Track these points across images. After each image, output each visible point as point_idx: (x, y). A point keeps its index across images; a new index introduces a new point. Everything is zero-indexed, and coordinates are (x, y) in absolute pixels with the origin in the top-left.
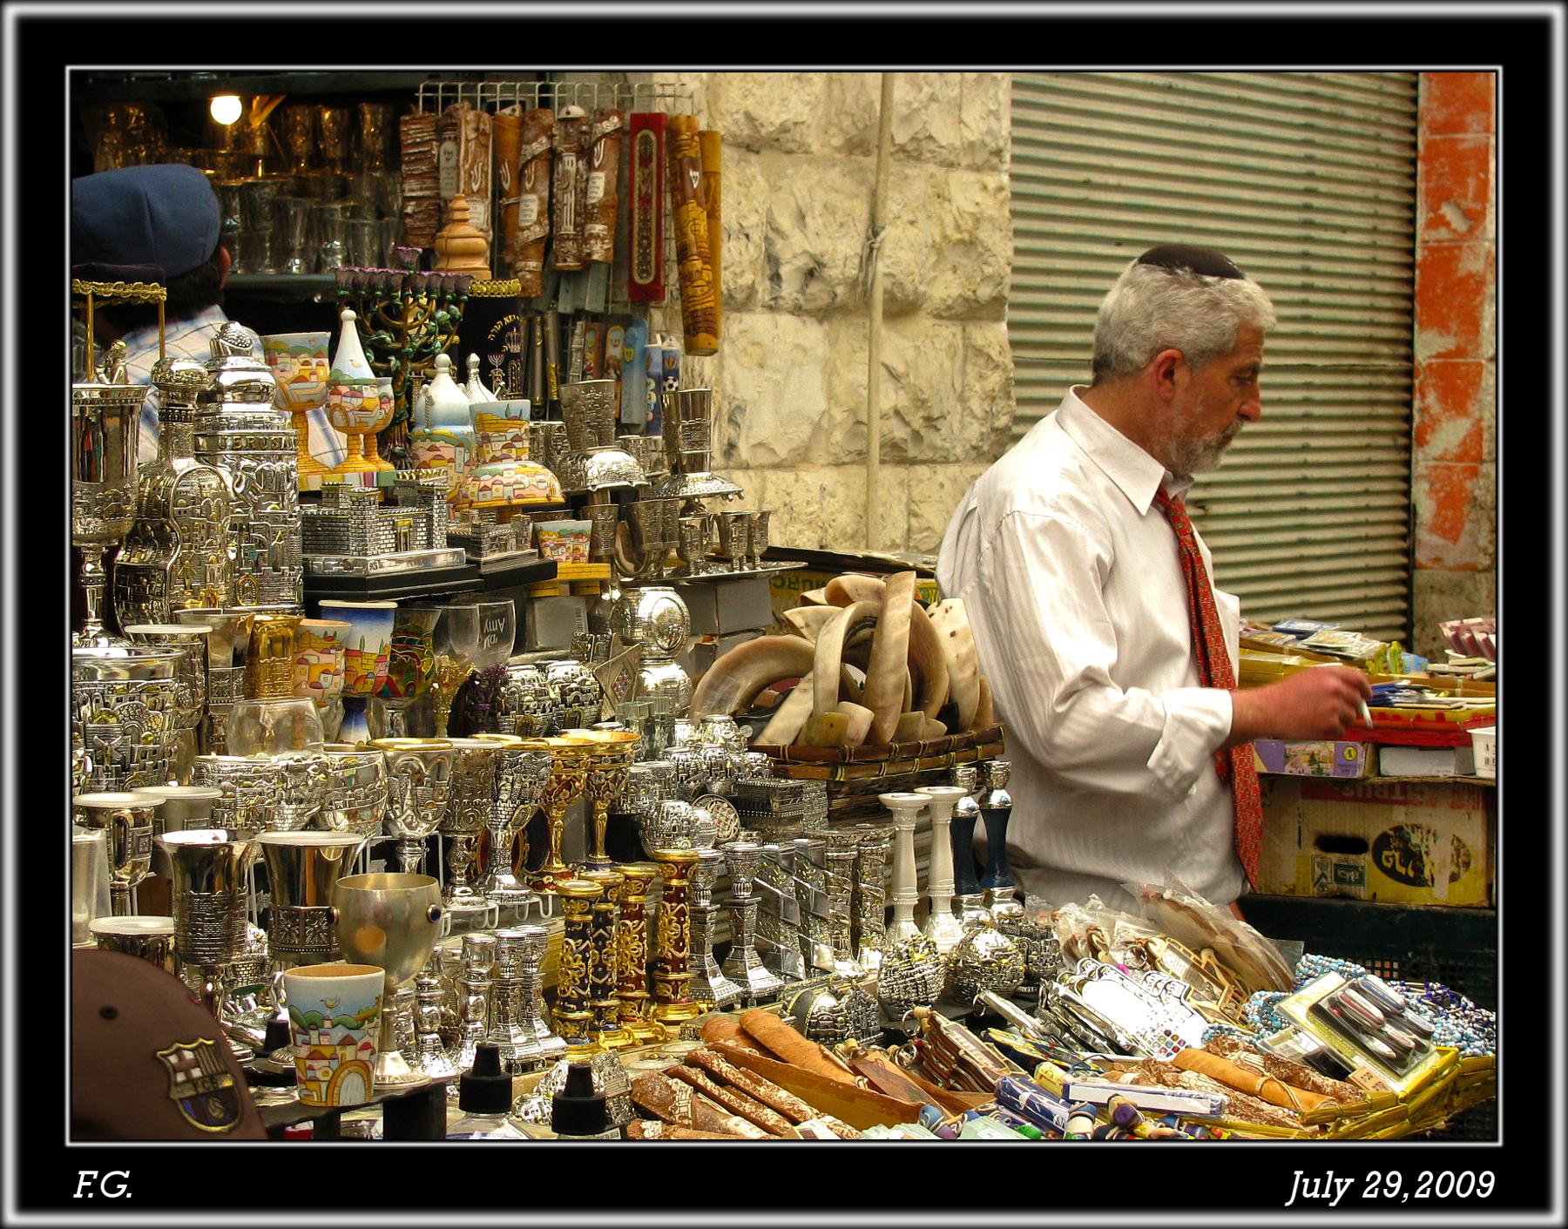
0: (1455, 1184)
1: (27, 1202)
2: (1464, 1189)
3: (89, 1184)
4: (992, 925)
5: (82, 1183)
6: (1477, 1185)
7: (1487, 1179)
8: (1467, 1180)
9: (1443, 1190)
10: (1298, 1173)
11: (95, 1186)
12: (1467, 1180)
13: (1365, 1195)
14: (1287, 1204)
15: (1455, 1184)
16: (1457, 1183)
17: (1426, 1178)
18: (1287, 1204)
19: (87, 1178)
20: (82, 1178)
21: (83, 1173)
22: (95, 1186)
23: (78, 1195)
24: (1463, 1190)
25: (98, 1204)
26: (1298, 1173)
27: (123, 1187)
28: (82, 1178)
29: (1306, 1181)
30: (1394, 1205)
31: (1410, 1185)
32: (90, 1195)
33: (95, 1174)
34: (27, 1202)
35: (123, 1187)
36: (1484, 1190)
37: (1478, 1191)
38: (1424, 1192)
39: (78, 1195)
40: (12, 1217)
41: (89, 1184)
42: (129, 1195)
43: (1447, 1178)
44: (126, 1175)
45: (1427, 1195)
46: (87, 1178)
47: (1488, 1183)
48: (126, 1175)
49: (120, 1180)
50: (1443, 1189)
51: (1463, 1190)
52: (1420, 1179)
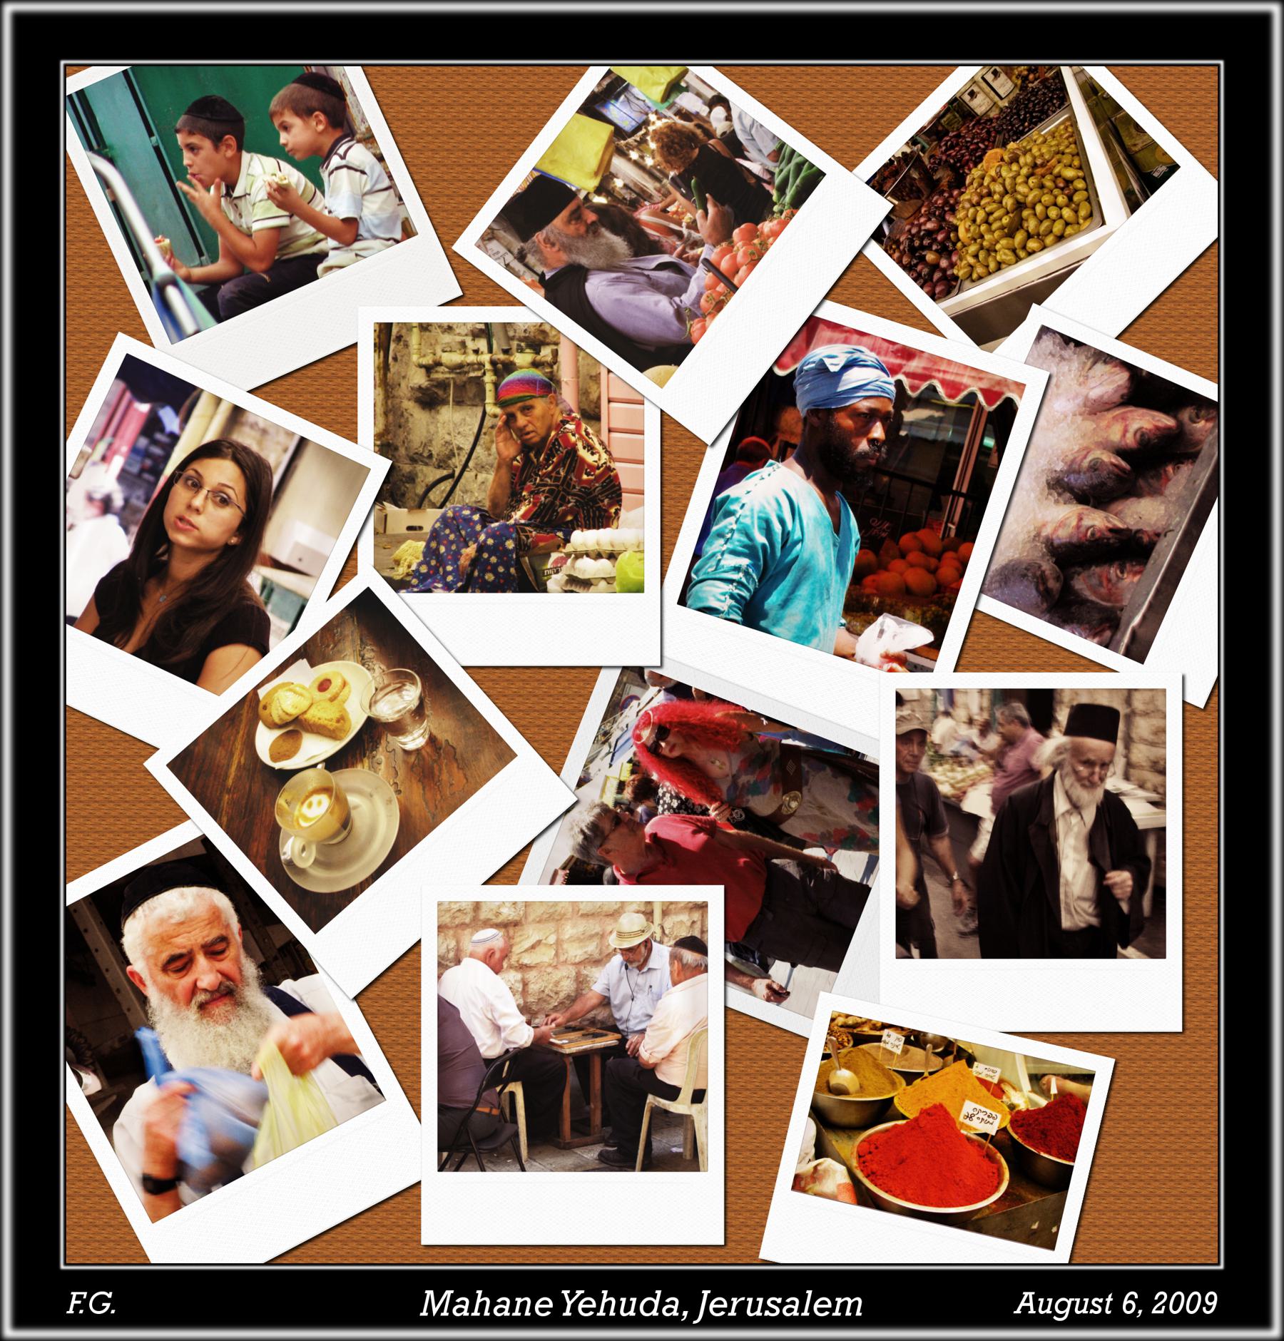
0: (1185, 1303)
1: (21, 1320)
3: (79, 1302)
5: (74, 1302)
6: (1203, 1304)
9: (1175, 1308)
10: (706, 1293)
11: (85, 1304)
12: (1195, 1299)
13: (1154, 1311)
14: (695, 1322)
15: (1185, 1303)
16: (1185, 1302)
17: (1161, 1297)
18: (695, 1322)
19: (78, 1298)
20: (74, 1298)
21: (74, 1294)
22: (85, 1304)
23: (71, 1311)
24: (1192, 1308)
26: (706, 1293)
27: (108, 1305)
28: (74, 1298)
29: (1041, 1300)
30: (673, 1323)
31: (1146, 1302)
32: (81, 1312)
33: (85, 1294)
34: (21, 1320)
35: (108, 1305)
36: (1209, 1308)
37: (1204, 1309)
38: (1159, 1308)
39: (71, 1311)
41: (79, 1302)
43: (1178, 1298)
44: (109, 1295)
45: (1162, 1312)
48: (109, 1295)
49: (104, 1299)
50: (1176, 1307)
51: (1192, 1308)
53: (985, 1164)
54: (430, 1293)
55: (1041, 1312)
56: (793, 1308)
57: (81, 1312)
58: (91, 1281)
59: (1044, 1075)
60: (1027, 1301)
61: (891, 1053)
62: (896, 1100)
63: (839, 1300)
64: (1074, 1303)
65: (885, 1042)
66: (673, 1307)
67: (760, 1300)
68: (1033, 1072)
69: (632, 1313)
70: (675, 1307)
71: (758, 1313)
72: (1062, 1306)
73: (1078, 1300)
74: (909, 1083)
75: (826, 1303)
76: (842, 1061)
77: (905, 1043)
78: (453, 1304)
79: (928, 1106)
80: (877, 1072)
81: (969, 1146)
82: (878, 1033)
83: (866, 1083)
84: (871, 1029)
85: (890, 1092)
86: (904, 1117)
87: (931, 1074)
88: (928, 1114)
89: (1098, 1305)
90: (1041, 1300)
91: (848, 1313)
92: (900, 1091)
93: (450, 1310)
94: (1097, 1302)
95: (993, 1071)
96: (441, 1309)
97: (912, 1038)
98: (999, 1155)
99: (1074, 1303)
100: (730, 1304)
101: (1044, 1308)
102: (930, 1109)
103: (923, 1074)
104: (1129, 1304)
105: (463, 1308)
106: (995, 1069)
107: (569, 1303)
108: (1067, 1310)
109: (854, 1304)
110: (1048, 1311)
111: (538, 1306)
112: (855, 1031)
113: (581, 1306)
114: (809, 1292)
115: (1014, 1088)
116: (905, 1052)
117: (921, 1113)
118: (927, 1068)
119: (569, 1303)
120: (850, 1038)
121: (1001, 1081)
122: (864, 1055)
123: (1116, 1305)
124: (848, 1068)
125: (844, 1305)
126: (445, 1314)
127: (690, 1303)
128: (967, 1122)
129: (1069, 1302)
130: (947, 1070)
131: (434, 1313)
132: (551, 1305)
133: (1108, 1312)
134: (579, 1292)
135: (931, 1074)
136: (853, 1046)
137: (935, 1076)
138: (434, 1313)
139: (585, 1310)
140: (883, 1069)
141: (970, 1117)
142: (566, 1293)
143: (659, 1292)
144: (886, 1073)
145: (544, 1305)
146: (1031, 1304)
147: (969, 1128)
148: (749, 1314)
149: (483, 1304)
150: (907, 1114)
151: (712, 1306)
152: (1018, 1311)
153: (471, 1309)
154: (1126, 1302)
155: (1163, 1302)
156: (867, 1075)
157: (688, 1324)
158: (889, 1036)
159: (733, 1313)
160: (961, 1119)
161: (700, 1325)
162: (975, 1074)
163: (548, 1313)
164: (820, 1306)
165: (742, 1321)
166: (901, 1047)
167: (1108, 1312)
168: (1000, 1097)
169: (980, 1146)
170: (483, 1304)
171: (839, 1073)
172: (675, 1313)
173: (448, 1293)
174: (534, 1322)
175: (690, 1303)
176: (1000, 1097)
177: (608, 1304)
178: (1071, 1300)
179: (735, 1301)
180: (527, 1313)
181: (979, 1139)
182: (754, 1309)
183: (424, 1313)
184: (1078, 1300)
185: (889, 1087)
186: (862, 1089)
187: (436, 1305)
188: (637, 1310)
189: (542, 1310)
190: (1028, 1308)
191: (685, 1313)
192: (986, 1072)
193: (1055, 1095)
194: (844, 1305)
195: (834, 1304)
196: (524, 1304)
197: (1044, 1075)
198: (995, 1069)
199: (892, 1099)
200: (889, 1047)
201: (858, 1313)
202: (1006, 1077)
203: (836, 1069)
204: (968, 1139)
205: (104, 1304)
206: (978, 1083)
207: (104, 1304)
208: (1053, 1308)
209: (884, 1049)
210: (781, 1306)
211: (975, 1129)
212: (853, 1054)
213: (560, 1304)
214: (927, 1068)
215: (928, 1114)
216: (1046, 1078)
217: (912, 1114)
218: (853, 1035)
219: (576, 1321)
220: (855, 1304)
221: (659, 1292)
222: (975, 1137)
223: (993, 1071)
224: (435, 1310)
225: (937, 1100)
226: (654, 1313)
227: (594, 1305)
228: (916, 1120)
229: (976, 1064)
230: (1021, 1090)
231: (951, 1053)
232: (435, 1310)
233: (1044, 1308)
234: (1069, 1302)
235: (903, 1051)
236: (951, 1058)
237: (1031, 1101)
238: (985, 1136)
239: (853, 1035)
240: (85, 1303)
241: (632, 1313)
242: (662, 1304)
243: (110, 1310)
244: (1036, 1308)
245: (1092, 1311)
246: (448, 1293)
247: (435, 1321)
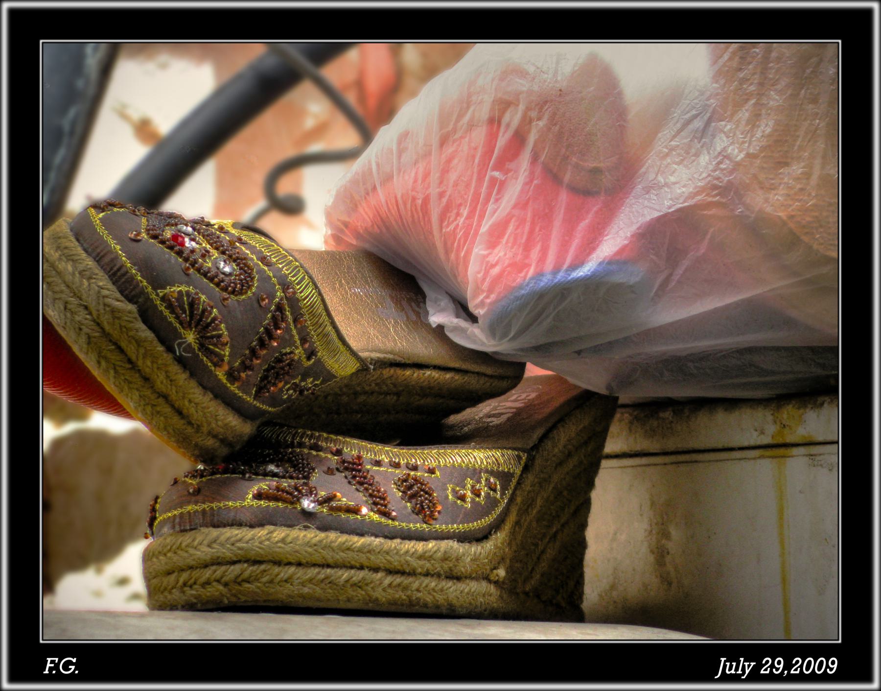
0: (814, 666)
3: (53, 665)
5: (49, 665)
6: (827, 666)
7: (833, 663)
9: (807, 669)
10: (723, 659)
12: (821, 663)
13: (762, 672)
14: (716, 677)
15: (814, 666)
16: (814, 665)
17: (797, 662)
18: (716, 677)
19: (52, 662)
20: (49, 662)
23: (47, 672)
26: (723, 659)
27: (73, 667)
28: (49, 662)
29: (728, 664)
31: (788, 666)
33: (57, 659)
35: (73, 667)
36: (831, 669)
37: (828, 670)
39: (47, 672)
41: (53, 665)
42: (77, 672)
43: (810, 662)
44: (74, 660)
45: (798, 672)
48: (74, 660)
51: (819, 669)
52: (794, 662)
57: (54, 672)
58: (61, 650)
205: (70, 667)
207: (70, 667)
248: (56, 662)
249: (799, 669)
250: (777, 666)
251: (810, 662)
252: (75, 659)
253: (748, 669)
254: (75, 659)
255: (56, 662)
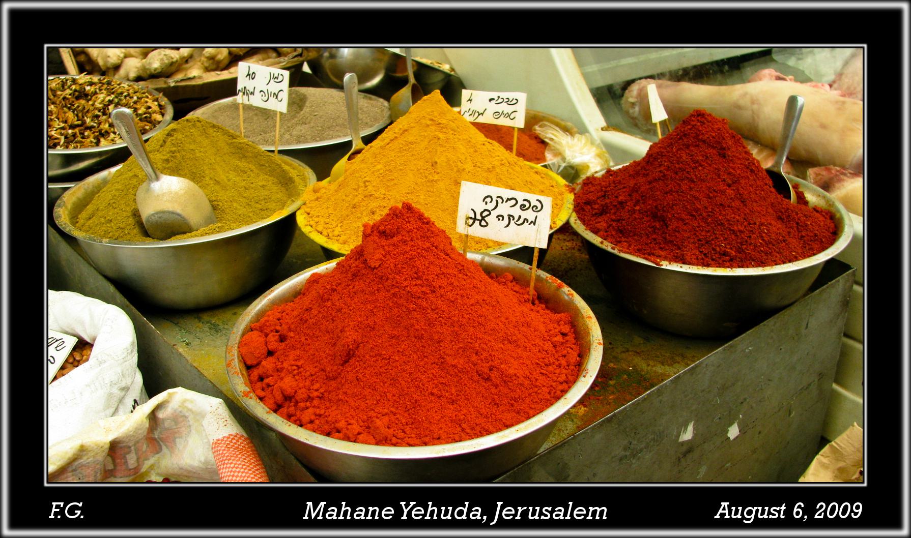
0: (839, 510)
2: (844, 513)
3: (58, 510)
4: (168, 168)
5: (54, 510)
6: (852, 511)
7: (858, 507)
8: (846, 508)
9: (831, 514)
12: (846, 508)
13: (816, 517)
14: (491, 524)
16: (839, 510)
17: (821, 507)
18: (491, 524)
19: (57, 507)
20: (54, 507)
23: (306, 518)
25: (63, 523)
26: (500, 504)
27: (79, 512)
28: (54, 507)
29: (733, 508)
30: (476, 525)
31: (810, 510)
33: (62, 504)
35: (79, 512)
36: (856, 514)
37: (852, 514)
38: (820, 515)
39: (52, 517)
40: (6, 532)
41: (58, 510)
42: (82, 517)
43: (834, 507)
44: (80, 505)
45: (822, 517)
46: (57, 507)
47: (858, 510)
49: (77, 508)
50: (832, 513)
51: (844, 514)
52: (818, 507)
53: (539, 318)
54: (310, 504)
55: (733, 517)
56: (560, 514)
57: (59, 517)
58: (67, 494)
59: (628, 84)
60: (724, 509)
61: (266, 114)
62: (301, 220)
63: (591, 509)
64: (757, 511)
65: (245, 92)
66: (477, 513)
67: (767, 508)
68: (602, 82)
69: (449, 517)
70: (479, 514)
71: (536, 517)
72: (750, 513)
73: (760, 508)
74: (322, 174)
75: (582, 511)
76: (157, 157)
77: (292, 84)
78: (325, 511)
79: (377, 218)
80: (242, 164)
81: (495, 287)
82: (225, 75)
83: (222, 196)
84: (207, 70)
85: (283, 206)
86: (329, 255)
87: (368, 140)
88: (383, 234)
89: (778, 511)
90: (733, 508)
91: (597, 518)
92: (307, 195)
93: (324, 515)
94: (546, 510)
95: (509, 102)
96: (318, 515)
97: (306, 68)
98: (566, 289)
99: (757, 511)
100: (517, 511)
101: (736, 514)
102: (382, 221)
103: (349, 144)
104: (798, 510)
105: (333, 514)
106: (511, 95)
107: (406, 511)
108: (753, 516)
109: (601, 511)
110: (739, 516)
111: (384, 512)
112: (172, 83)
113: (414, 512)
114: (571, 503)
115: (566, 130)
116: (297, 103)
117: (366, 236)
118: (356, 131)
119: (406, 511)
120: (164, 101)
121: (533, 120)
122: (204, 132)
123: (789, 512)
124: (175, 171)
125: (594, 512)
126: (320, 518)
127: (489, 511)
128: (476, 231)
129: (754, 510)
130: (402, 123)
131: (313, 518)
132: (393, 512)
133: (782, 517)
134: (412, 503)
135: (368, 140)
136: (177, 116)
137: (376, 143)
138: (313, 518)
139: (416, 515)
140: (258, 155)
141: (481, 219)
142: (403, 503)
143: (467, 503)
144: (263, 162)
145: (388, 512)
146: (726, 511)
147: (483, 244)
148: (530, 517)
149: (346, 512)
150: (334, 246)
151: (504, 512)
152: (717, 517)
153: (338, 515)
154: (795, 510)
155: (822, 510)
156: (222, 177)
157: (487, 526)
158: (251, 76)
159: (518, 518)
160: (461, 228)
161: (496, 527)
162: (469, 118)
163: (391, 517)
164: (579, 512)
165: (525, 523)
166: (284, 96)
167: (782, 517)
168: (540, 158)
169: (519, 280)
170: (346, 512)
171: (156, 186)
172: (479, 518)
173: (323, 504)
174: (381, 524)
175: (489, 511)
176: (540, 158)
177: (433, 512)
178: (756, 508)
179: (520, 509)
180: (377, 518)
181: (513, 263)
182: (533, 514)
183: (306, 518)
184: (760, 508)
185: (277, 192)
186: (216, 212)
187: (314, 511)
188: (452, 515)
189: (386, 515)
190: (725, 514)
191: (485, 518)
192: (493, 107)
193: (663, 123)
194: (594, 512)
195: (588, 511)
196: (374, 512)
197: (628, 84)
198: (511, 95)
199: (291, 218)
200: (256, 101)
201: (605, 518)
202: (542, 108)
203: (149, 179)
204: (490, 271)
205: (76, 512)
206: (480, 137)
207: (76, 512)
208: (742, 514)
209: (249, 108)
210: (551, 513)
211: (500, 244)
212: (179, 136)
213: (399, 511)
214: (356, 131)
215: (383, 234)
216: (635, 89)
217: (344, 245)
218: (168, 92)
219: (411, 524)
220: (602, 512)
221: (467, 503)
222: (502, 262)
223: (509, 102)
224: (313, 515)
225: (396, 199)
226: (464, 517)
227: (423, 512)
228: (358, 253)
229: (465, 93)
230: (582, 130)
231: (404, 82)
232: (313, 515)
233: (736, 514)
234: (754, 510)
235: (291, 103)
236: (405, 92)
237: (612, 150)
238: (524, 253)
239: (168, 92)
240: (63, 510)
241: (449, 517)
242: (469, 511)
243: (80, 516)
244: (730, 514)
245: (771, 517)
246: (323, 504)
247: (314, 524)
248: (62, 506)
249: (823, 513)
250: (800, 510)
251: (834, 507)
252: (81, 503)
253: (314, 512)
254: (81, 503)
255: (62, 506)
